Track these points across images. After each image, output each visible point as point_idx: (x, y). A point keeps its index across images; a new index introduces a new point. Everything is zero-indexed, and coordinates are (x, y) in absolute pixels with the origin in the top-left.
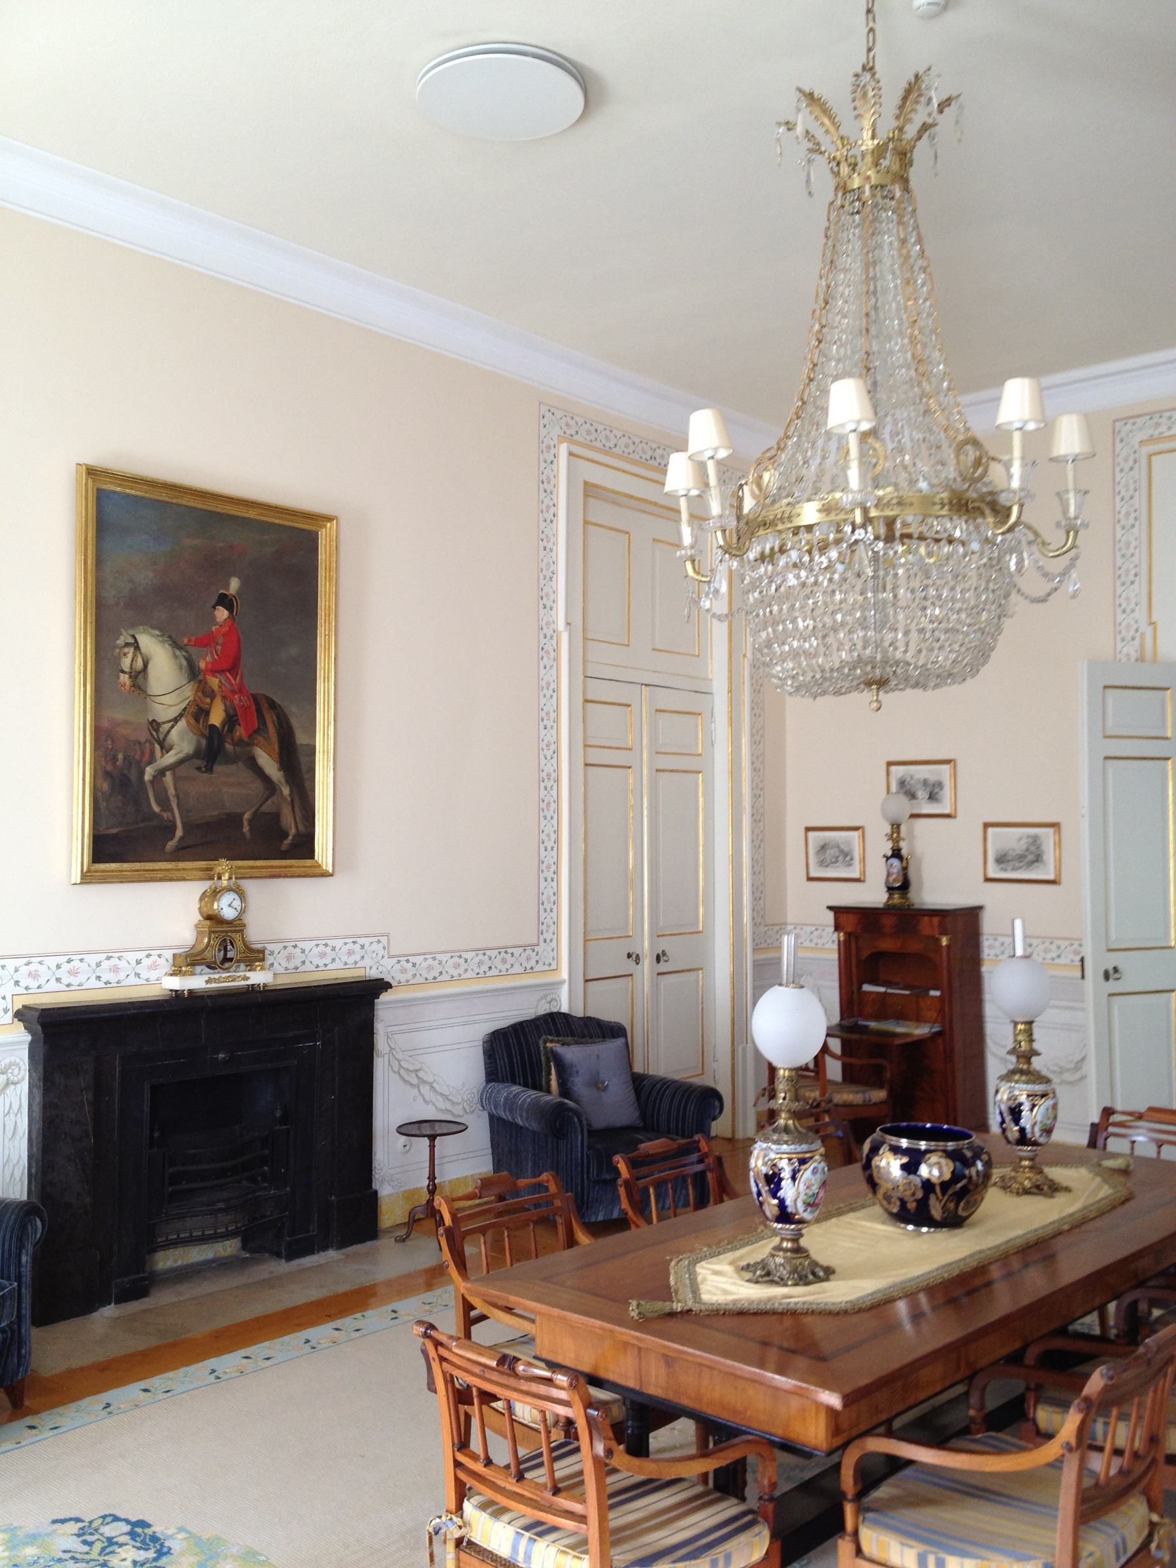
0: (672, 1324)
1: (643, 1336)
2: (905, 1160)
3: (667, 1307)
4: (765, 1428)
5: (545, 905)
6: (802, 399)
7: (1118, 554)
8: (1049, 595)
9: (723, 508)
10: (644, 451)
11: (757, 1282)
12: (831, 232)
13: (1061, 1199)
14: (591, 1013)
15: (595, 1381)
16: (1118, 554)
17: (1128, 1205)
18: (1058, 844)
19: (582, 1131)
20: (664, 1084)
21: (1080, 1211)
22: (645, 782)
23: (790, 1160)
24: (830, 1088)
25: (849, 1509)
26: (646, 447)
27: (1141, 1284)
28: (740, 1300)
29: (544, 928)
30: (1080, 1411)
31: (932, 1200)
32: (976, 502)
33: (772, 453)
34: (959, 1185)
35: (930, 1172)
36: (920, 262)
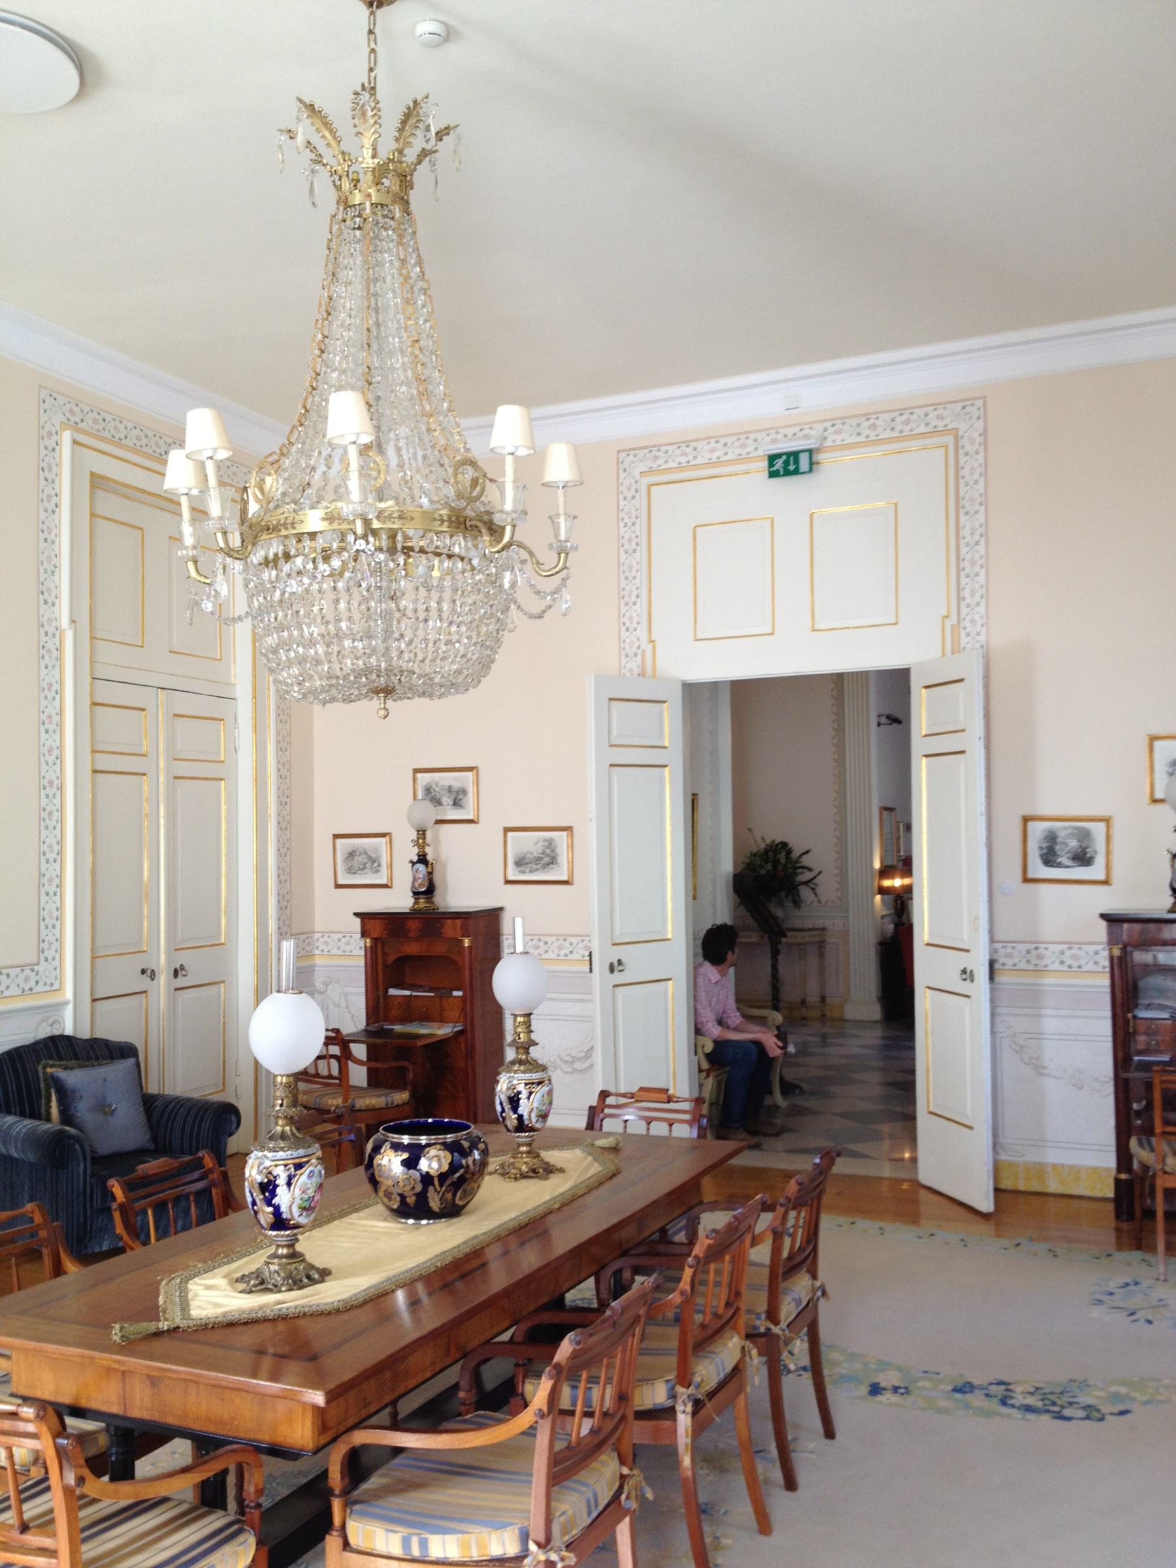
0: (158, 1345)
1: (126, 1359)
2: (405, 1156)
3: (152, 1327)
4: (252, 1436)
5: (47, 921)
6: (305, 407)
7: (622, 576)
8: (544, 612)
9: (223, 510)
10: (158, 446)
11: (251, 1292)
12: (333, 245)
13: (555, 1179)
14: (100, 1034)
15: (78, 1412)
16: (622, 576)
17: (615, 1180)
18: (571, 846)
19: (85, 1159)
20: (178, 1103)
21: (570, 1189)
22: (161, 789)
23: (286, 1166)
24: (352, 1095)
25: (336, 1505)
26: (159, 440)
27: (625, 1253)
28: (230, 1312)
29: (45, 945)
30: (551, 1377)
31: (431, 1193)
32: (473, 521)
33: (275, 457)
34: (457, 1175)
35: (430, 1166)
36: (420, 284)
